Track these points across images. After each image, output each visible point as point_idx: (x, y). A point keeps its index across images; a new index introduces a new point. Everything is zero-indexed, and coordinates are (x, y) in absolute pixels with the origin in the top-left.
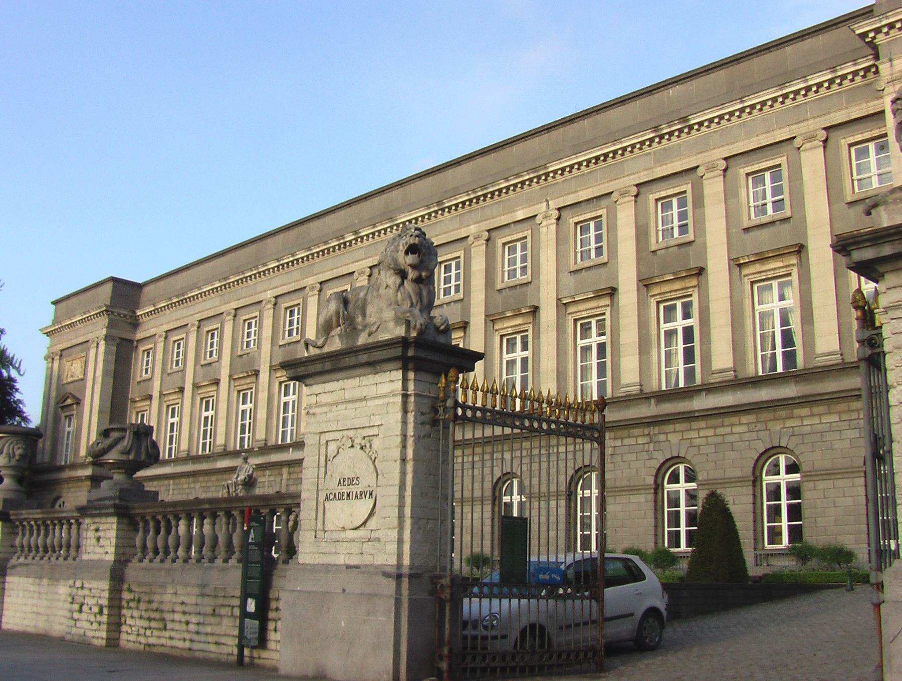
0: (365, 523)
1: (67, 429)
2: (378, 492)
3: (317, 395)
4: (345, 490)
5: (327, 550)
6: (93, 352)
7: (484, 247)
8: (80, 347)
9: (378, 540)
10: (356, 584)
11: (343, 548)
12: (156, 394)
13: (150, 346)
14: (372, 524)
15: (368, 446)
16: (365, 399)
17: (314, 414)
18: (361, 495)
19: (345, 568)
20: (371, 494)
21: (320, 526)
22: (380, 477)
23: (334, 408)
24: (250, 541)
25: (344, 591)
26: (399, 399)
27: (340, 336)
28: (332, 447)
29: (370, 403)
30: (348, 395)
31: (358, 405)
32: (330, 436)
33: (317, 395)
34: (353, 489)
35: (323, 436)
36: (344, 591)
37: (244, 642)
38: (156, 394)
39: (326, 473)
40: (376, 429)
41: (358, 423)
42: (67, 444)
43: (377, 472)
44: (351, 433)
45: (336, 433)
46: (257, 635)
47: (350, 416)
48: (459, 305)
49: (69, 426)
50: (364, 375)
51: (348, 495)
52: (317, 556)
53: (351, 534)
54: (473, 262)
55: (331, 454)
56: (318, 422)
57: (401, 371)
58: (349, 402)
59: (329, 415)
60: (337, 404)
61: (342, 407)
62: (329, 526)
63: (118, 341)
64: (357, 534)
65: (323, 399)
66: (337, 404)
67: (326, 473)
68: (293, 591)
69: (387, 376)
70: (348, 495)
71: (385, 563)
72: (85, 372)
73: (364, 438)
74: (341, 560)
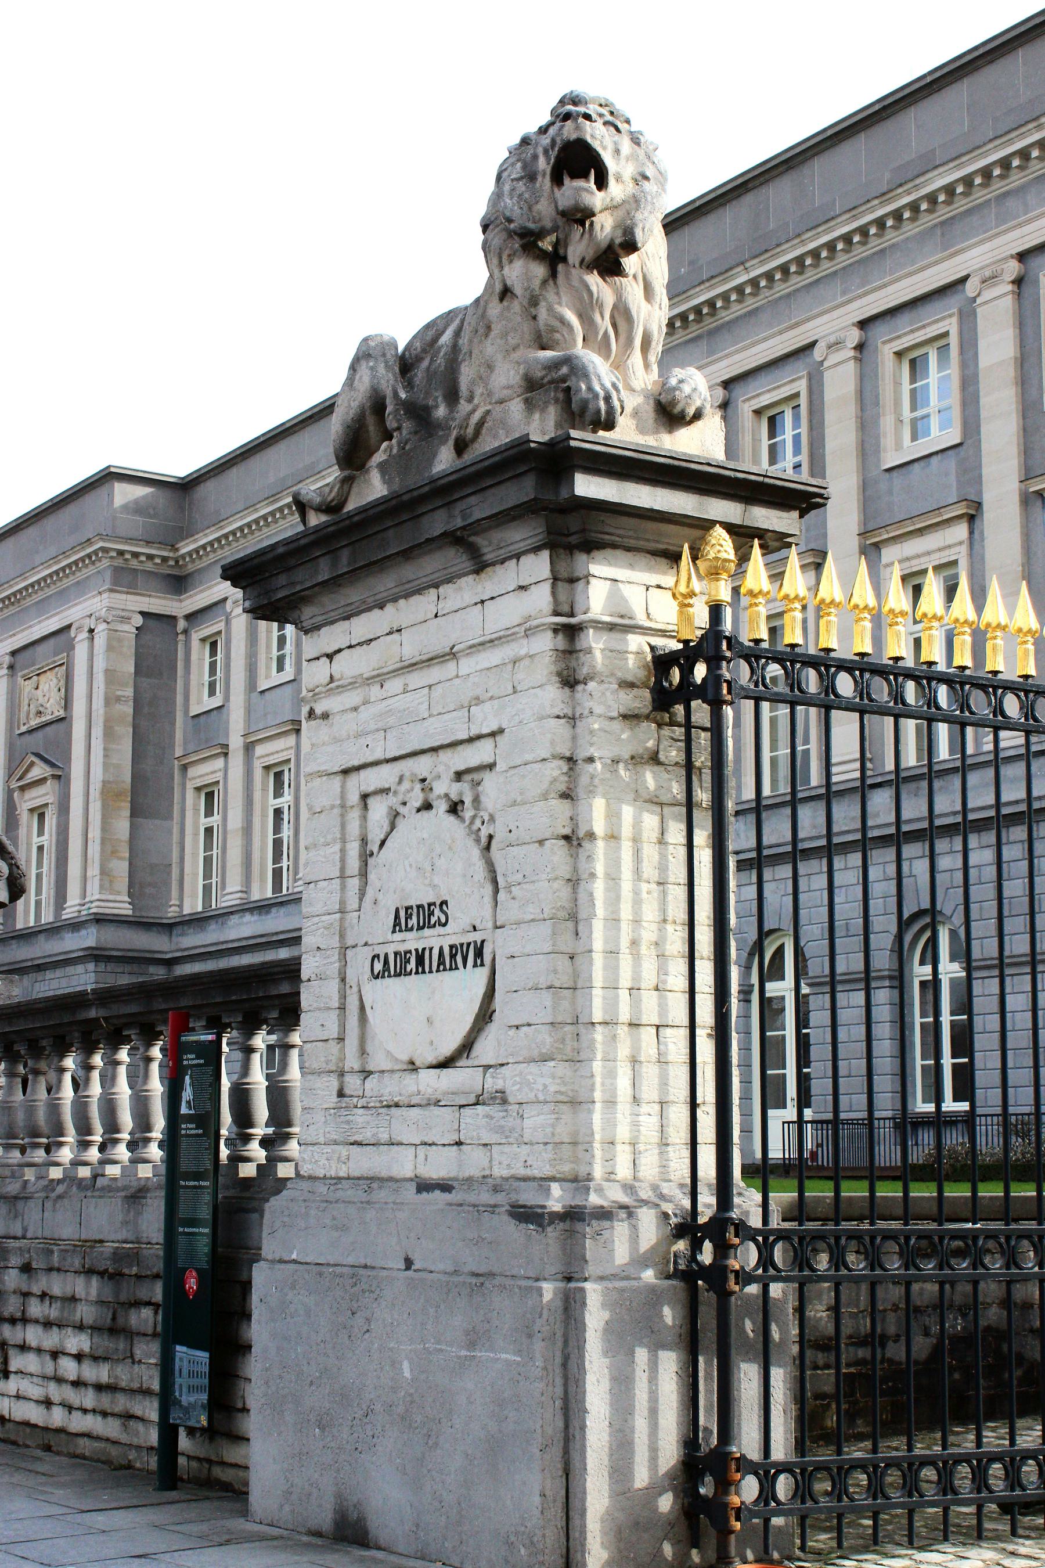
0: (467, 1047)
1: (36, 840)
2: (498, 945)
3: (330, 657)
4: (413, 942)
5: (366, 1135)
6: (81, 652)
7: (1008, 302)
8: (52, 642)
9: (501, 1098)
10: (443, 1245)
11: (406, 1126)
12: (236, 742)
13: (214, 629)
14: (486, 1049)
15: (468, 800)
16: (452, 654)
17: (325, 716)
18: (454, 958)
19: (412, 1187)
20: (479, 953)
21: (352, 1062)
22: (501, 896)
23: (375, 691)
24: (184, 1110)
25: (409, 1263)
26: (545, 643)
27: (382, 467)
28: (379, 809)
29: (467, 665)
30: (410, 647)
31: (435, 673)
32: (371, 780)
33: (330, 657)
34: (434, 940)
35: (353, 780)
36: (409, 1263)
37: (175, 1416)
38: (236, 742)
39: (362, 893)
40: (487, 744)
41: (435, 732)
42: (39, 877)
43: (495, 882)
44: (422, 766)
45: (385, 769)
46: (204, 1397)
47: (419, 710)
48: (951, 462)
49: (41, 832)
50: (449, 581)
51: (420, 960)
52: (344, 1151)
53: (431, 1082)
54: (982, 345)
55: (375, 835)
56: (336, 740)
57: (545, 554)
58: (413, 666)
59: (365, 713)
60: (380, 678)
61: (394, 685)
62: (378, 1061)
63: (139, 621)
64: (449, 1078)
65: (347, 666)
66: (380, 678)
67: (362, 893)
68: (281, 1261)
69: (505, 576)
70: (420, 960)
71: (522, 1172)
72: (67, 703)
73: (459, 776)
74: (404, 1164)
